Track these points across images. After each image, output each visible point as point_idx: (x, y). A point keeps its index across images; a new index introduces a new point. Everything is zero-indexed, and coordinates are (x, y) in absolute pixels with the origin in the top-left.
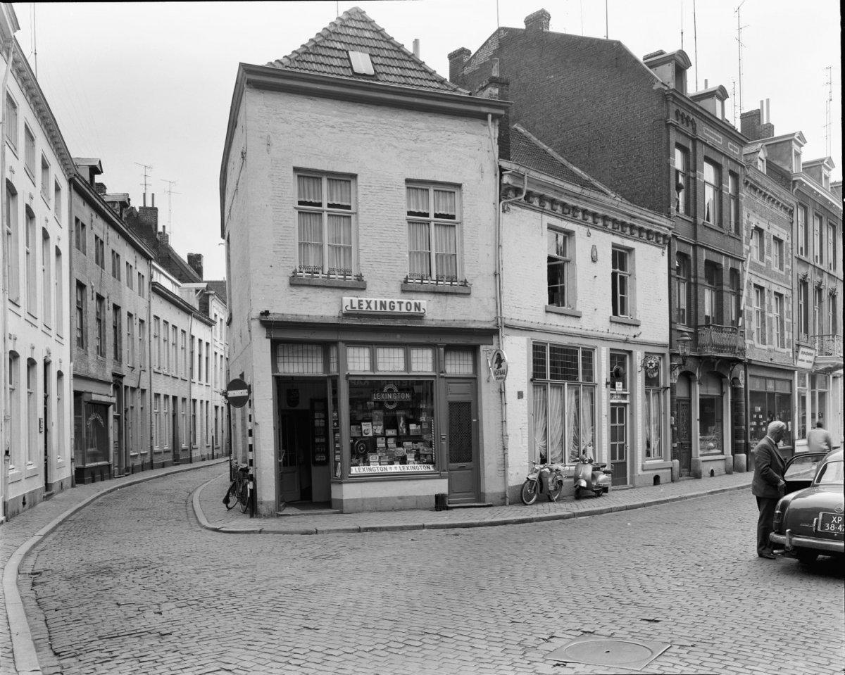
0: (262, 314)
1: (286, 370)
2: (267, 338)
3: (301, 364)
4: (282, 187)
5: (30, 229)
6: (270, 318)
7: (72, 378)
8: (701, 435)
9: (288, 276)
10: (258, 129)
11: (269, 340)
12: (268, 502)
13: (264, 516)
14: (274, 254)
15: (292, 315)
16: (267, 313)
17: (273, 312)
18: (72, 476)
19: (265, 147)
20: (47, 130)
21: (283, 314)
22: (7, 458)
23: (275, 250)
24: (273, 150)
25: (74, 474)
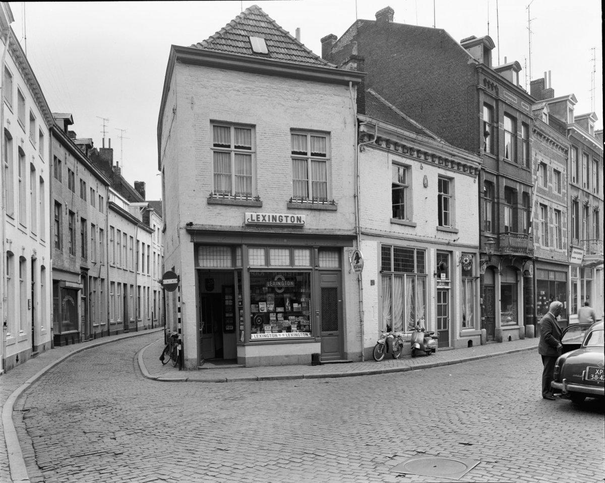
0: (188, 225)
1: (205, 265)
2: (191, 242)
3: (215, 261)
4: (202, 134)
5: (21, 164)
6: (194, 227)
7: (52, 270)
8: (502, 311)
9: (206, 198)
10: (185, 92)
11: (193, 244)
12: (192, 359)
13: (189, 369)
14: (196, 182)
15: (209, 225)
16: (191, 224)
17: (196, 223)
18: (52, 341)
19: (190, 105)
20: (34, 93)
21: (203, 225)
22: (5, 327)
23: (197, 179)
24: (195, 107)
25: (53, 339)
